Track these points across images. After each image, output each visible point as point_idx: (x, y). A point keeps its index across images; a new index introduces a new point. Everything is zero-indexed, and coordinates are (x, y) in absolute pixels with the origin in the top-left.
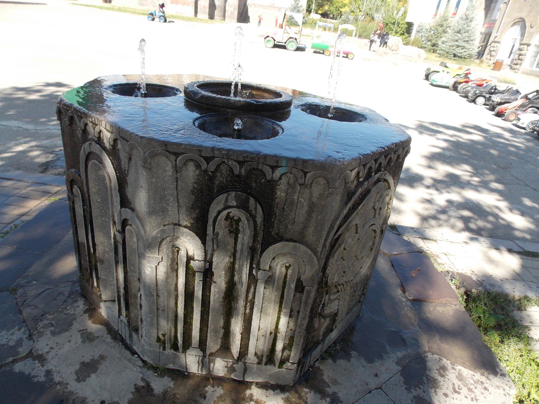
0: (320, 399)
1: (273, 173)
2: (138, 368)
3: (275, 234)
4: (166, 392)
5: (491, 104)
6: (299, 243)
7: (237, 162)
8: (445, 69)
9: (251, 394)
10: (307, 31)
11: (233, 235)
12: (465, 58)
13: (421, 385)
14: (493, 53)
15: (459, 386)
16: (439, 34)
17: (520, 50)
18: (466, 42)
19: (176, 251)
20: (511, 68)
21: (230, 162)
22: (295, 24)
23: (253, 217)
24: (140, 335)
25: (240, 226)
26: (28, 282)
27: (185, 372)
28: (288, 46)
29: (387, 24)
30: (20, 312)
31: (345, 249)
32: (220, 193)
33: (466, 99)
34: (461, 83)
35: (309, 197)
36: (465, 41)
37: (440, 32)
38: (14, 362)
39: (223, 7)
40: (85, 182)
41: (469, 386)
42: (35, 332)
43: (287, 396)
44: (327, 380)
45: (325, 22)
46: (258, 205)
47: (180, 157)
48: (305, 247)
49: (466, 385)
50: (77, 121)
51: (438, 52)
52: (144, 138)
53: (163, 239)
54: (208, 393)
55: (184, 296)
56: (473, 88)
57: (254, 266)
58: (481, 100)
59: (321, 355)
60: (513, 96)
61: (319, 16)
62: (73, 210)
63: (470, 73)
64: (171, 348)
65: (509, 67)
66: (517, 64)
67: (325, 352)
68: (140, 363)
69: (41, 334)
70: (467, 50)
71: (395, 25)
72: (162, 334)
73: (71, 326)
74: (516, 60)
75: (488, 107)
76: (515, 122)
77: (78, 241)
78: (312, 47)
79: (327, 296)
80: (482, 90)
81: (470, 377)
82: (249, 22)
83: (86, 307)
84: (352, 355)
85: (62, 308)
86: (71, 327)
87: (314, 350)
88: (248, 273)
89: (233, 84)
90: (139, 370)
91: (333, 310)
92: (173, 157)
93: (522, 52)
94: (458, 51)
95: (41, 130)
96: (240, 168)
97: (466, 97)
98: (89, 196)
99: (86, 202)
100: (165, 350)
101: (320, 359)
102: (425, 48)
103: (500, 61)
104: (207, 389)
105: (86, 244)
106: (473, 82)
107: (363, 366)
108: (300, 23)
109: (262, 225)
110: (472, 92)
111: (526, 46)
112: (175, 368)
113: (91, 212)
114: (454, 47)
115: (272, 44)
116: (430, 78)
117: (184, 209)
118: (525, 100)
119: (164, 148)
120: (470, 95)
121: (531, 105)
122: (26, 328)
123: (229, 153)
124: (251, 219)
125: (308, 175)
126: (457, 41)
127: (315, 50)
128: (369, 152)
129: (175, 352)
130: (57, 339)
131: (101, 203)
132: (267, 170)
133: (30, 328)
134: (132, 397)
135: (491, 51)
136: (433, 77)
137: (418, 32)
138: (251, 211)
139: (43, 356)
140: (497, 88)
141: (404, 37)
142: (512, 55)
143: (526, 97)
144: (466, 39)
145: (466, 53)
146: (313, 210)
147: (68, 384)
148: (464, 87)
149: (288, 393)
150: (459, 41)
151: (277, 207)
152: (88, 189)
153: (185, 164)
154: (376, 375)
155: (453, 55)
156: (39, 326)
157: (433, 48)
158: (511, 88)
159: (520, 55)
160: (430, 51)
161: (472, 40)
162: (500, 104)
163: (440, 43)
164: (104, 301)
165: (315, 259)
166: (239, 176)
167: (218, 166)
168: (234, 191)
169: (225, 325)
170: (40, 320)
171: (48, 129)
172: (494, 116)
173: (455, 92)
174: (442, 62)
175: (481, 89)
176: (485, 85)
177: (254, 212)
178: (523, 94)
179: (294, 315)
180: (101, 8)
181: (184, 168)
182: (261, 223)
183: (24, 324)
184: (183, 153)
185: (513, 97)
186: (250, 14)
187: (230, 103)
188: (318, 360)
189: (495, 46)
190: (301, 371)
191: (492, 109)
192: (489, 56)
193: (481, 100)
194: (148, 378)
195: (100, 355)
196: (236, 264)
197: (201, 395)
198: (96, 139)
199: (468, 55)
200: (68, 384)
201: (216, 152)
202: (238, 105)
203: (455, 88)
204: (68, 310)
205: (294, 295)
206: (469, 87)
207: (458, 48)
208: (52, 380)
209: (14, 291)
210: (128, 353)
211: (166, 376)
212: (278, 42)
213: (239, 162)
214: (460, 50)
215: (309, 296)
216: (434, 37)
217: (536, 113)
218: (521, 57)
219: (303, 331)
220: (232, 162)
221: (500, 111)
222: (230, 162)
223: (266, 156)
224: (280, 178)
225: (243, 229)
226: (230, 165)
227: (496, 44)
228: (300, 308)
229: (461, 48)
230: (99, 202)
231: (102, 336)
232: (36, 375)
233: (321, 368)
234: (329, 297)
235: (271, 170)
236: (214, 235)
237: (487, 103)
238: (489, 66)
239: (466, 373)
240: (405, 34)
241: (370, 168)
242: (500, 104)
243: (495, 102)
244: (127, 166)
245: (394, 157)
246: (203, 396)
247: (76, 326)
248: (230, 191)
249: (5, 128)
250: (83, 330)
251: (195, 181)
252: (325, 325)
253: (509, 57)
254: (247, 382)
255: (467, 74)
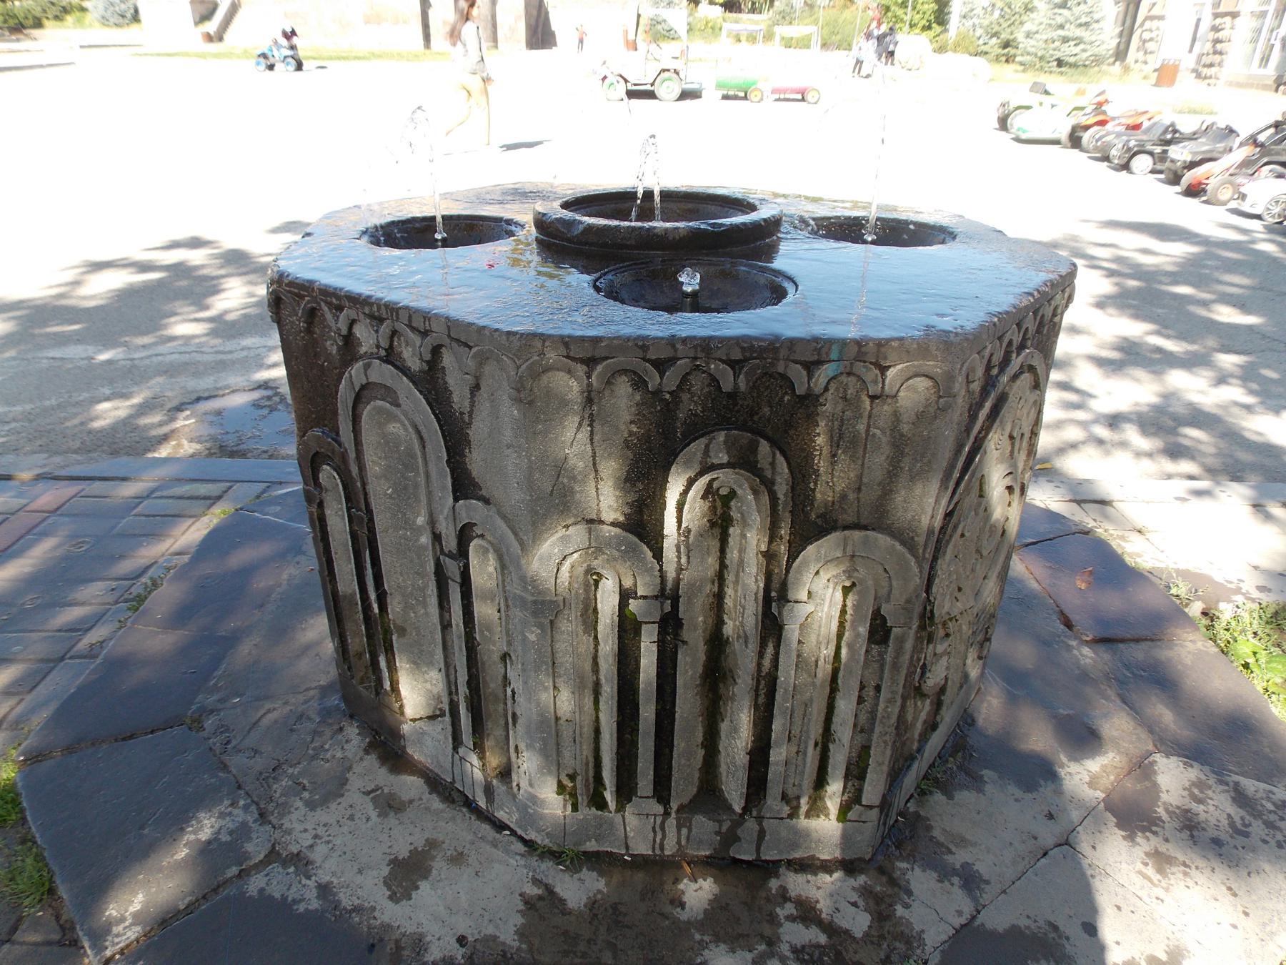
0: (938, 881)
1: (810, 376)
2: (518, 858)
3: (818, 517)
4: (594, 903)
5: (1170, 170)
6: (874, 529)
7: (729, 365)
8: (1044, 98)
9: (781, 886)
10: (698, 47)
11: (717, 531)
12: (1085, 66)
13: (1157, 825)
14: (1150, 46)
15: (1242, 818)
16: (1017, 16)
17: (1215, 29)
18: (1083, 28)
19: (592, 582)
20: (1199, 76)
21: (713, 366)
22: (665, 36)
23: (769, 484)
24: (514, 784)
25: (734, 508)
26: (221, 701)
27: (624, 855)
28: (660, 90)
29: (888, 9)
30: (225, 767)
31: (962, 535)
32: (689, 438)
33: (1106, 163)
34: (1087, 128)
35: (893, 423)
36: (1080, 25)
37: (1017, 10)
38: (242, 874)
39: (490, 18)
40: (352, 455)
41: (1265, 817)
42: (271, 807)
43: (862, 883)
44: (941, 839)
45: (736, 22)
46: (778, 453)
47: (599, 368)
48: (888, 539)
49: (1257, 815)
50: (329, 316)
51: (1018, 59)
52: (515, 333)
53: (564, 558)
54: (687, 895)
55: (616, 682)
56: (1119, 135)
57: (773, 594)
58: (1142, 163)
59: (918, 787)
60: (1220, 142)
61: (719, 9)
62: (320, 524)
63: (1107, 101)
64: (589, 806)
65: (1194, 75)
66: (1211, 65)
67: (925, 777)
68: (520, 847)
69: (284, 809)
70: (1089, 47)
71: (907, 7)
72: (567, 775)
73: (345, 784)
74: (1208, 54)
75: (1162, 176)
76: (1233, 205)
77: (335, 593)
78: (719, 86)
79: (931, 646)
80: (1145, 138)
81: (1264, 796)
82: (555, 45)
83: (368, 740)
84: (986, 779)
85: (314, 749)
86: (348, 787)
87: (905, 775)
88: (760, 613)
89: (439, 219)
90: (523, 863)
91: (938, 680)
92: (581, 369)
93: (1220, 35)
94: (1067, 51)
95: (142, 359)
96: (736, 377)
97: (1106, 158)
98: (364, 484)
99: (356, 499)
100: (577, 811)
101: (916, 795)
102: (986, 53)
103: (1171, 63)
104: (681, 886)
105: (358, 596)
106: (1117, 122)
107: (1017, 800)
108: (682, 29)
109: (789, 499)
110: (1120, 146)
111: (1228, 19)
112: (601, 849)
113: (371, 520)
114: (1057, 44)
115: (621, 89)
116: (1011, 125)
117: (610, 484)
118: (1252, 147)
119: (563, 351)
120: (1114, 152)
121: (1265, 160)
122: (249, 801)
123: (706, 346)
124: (763, 488)
125: (891, 373)
126: (1061, 27)
127: (725, 92)
128: (1005, 308)
129: (600, 813)
130: (321, 815)
131: (394, 499)
132: (797, 374)
133: (256, 799)
134: (523, 921)
135: (1145, 41)
136: (1016, 122)
137: (964, 17)
138: (762, 470)
139: (302, 855)
140: (1178, 127)
141: (931, 33)
142: (1198, 45)
143: (1253, 140)
144: (1083, 20)
145: (1088, 54)
146: (903, 452)
147: (373, 909)
148: (1097, 137)
149: (863, 876)
150: (1067, 26)
151: (820, 454)
152: (362, 468)
153: (609, 383)
154: (1050, 816)
155: (1055, 63)
156: (275, 792)
157: (1006, 51)
158: (1213, 124)
159: (1217, 41)
160: (997, 59)
161: (1097, 21)
162: (1192, 165)
163: (1020, 36)
164: (411, 720)
165: (913, 562)
166: (733, 395)
167: (685, 379)
168: (723, 430)
169: (705, 739)
170: (274, 778)
171: (156, 355)
172: (1180, 196)
173: (1076, 151)
174: (1035, 83)
175: (1139, 135)
176: (1146, 125)
177: (768, 474)
178: (1244, 134)
179: (868, 696)
180: (202, 56)
181: (607, 393)
182: (785, 495)
183: (242, 792)
184: (606, 358)
185: (1220, 146)
186: (555, 25)
187: (657, 235)
188: (912, 796)
189: (1154, 29)
190: (885, 824)
191: (1175, 179)
192: (1141, 53)
193: (1142, 163)
194: (546, 876)
195: (427, 840)
196: (727, 597)
197: (672, 902)
198: (383, 353)
199: (1092, 58)
200: (373, 909)
201: (679, 347)
202: (674, 239)
203: (1075, 140)
204: (328, 750)
205: (867, 651)
206: (1108, 134)
207: (1067, 45)
208: (337, 905)
209: (196, 724)
210: (486, 828)
211: (584, 869)
212: (635, 85)
213: (733, 364)
214: (1072, 48)
215: (901, 648)
216: (1005, 25)
217: (1280, 176)
218: (1219, 46)
219: (890, 730)
220: (717, 367)
221: (1194, 182)
222: (713, 366)
223: (792, 343)
224: (826, 389)
225: (742, 514)
226: (712, 372)
227: (1155, 23)
228: (881, 679)
229: (1074, 43)
230: (390, 496)
231: (421, 799)
232: (298, 897)
233: (922, 813)
234: (935, 648)
235: (804, 373)
236: (679, 534)
237: (1159, 167)
238: (1145, 78)
239: (1253, 789)
240: (934, 25)
241: (1010, 343)
242: (1192, 165)
243: (1179, 164)
244: (467, 403)
245: (1048, 311)
246: (677, 903)
247: (356, 782)
248: (714, 431)
249: (59, 363)
250: (373, 791)
251: (633, 418)
252: (923, 715)
253: (1191, 51)
254: (767, 862)
255: (1100, 104)
